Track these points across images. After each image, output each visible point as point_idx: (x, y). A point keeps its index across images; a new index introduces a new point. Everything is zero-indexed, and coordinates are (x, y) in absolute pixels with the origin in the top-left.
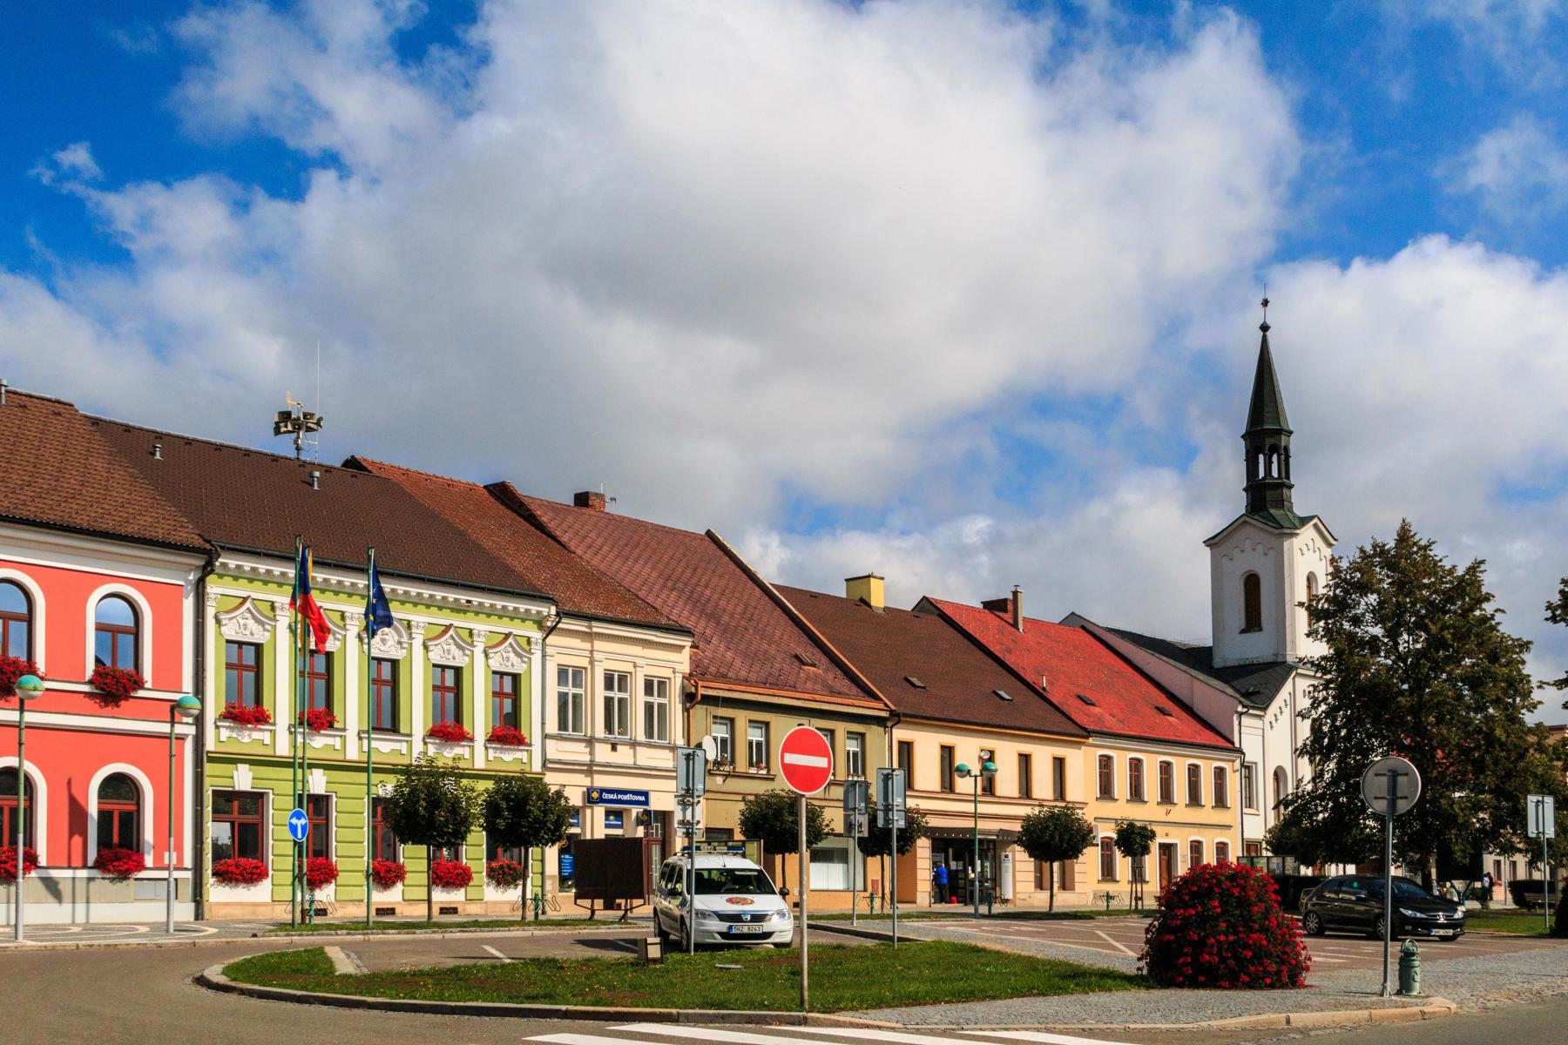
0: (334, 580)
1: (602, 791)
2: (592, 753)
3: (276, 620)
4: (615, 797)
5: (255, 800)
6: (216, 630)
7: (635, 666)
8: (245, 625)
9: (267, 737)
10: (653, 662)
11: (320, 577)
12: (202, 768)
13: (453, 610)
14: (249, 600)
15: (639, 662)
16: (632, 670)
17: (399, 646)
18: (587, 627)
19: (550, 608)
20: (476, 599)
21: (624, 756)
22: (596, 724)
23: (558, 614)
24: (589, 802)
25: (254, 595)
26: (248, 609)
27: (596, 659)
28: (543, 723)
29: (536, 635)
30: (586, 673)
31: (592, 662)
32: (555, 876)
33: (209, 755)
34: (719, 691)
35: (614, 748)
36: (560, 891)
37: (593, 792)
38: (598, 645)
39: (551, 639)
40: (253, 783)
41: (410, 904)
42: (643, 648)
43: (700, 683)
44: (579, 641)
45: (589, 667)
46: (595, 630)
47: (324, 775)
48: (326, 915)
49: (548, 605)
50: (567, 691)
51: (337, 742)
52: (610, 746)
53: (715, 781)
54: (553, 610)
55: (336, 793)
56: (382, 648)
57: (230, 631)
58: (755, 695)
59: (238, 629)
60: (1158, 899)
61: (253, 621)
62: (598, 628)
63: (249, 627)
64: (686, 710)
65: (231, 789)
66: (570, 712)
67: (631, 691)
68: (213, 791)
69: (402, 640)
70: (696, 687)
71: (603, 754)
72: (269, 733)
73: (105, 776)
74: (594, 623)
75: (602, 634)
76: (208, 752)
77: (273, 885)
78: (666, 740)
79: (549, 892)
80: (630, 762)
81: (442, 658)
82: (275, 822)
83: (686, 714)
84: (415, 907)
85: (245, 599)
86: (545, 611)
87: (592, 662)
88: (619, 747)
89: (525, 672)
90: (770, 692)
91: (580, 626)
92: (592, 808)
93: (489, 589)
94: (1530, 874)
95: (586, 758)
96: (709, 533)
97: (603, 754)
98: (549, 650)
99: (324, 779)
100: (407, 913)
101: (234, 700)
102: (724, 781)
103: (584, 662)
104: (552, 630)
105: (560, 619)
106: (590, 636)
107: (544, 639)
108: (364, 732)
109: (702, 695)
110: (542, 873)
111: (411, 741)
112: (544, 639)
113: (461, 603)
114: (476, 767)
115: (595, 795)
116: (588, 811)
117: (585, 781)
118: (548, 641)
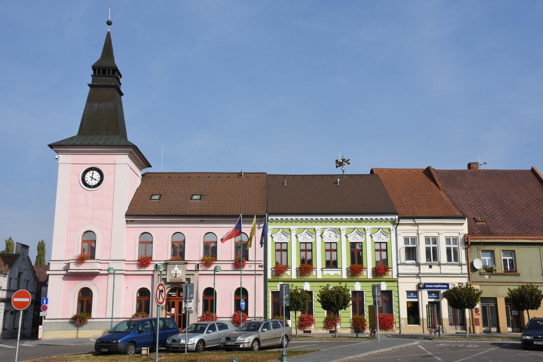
0: (344, 218)
1: (425, 284)
2: (420, 269)
3: (366, 234)
4: (432, 286)
5: (361, 293)
6: (321, 240)
7: (439, 234)
8: (380, 237)
9: (339, 273)
10: (426, 231)
11: (329, 218)
12: (266, 284)
13: (355, 222)
14: (306, 229)
15: (440, 232)
16: (438, 235)
17: (336, 237)
18: (413, 221)
19: (395, 217)
20: (364, 218)
21: (435, 269)
22: (422, 257)
23: (399, 218)
24: (419, 289)
25: (382, 227)
26: (381, 231)
27: (242, 231)
28: (397, 260)
29: (391, 227)
30: (417, 238)
31: (418, 234)
32: (405, 318)
33: (269, 280)
34: (481, 240)
35: (430, 267)
36: (408, 324)
37: (420, 285)
38: (421, 227)
39: (399, 227)
40: (361, 288)
41: (343, 329)
42: (412, 226)
43: (469, 238)
44: (411, 226)
45: (417, 236)
46: (417, 222)
47: (385, 284)
48: (311, 332)
49: (395, 216)
50: (450, 246)
51: (339, 273)
52: (428, 266)
53: (485, 277)
54: (397, 217)
55: (314, 290)
56: (330, 239)
57: (276, 240)
58: (502, 240)
59: (303, 238)
60: (327, 330)
61: (383, 235)
62: (418, 221)
63: (382, 237)
64: (466, 249)
65: (277, 291)
66: (411, 253)
67: (438, 244)
68: (271, 291)
69: (337, 235)
70: (468, 239)
71: (425, 269)
72: (289, 271)
73: (204, 289)
74: (416, 220)
75: (422, 223)
76: (268, 279)
77: (292, 322)
78: (437, 261)
79: (403, 324)
80: (438, 272)
81: (278, 240)
82: (366, 301)
83: (466, 250)
84: (345, 330)
85: (380, 228)
86: (393, 217)
87: (418, 234)
88: (433, 266)
89: (389, 241)
90: (512, 237)
91: (411, 221)
92: (421, 291)
93: (369, 213)
94: (519, 313)
95: (417, 272)
96: (533, 171)
97: (425, 269)
98: (398, 232)
99: (386, 285)
100: (342, 332)
101: (279, 261)
102: (489, 277)
103: (415, 235)
104: (398, 224)
105: (399, 220)
106: (417, 225)
107: (396, 228)
108: (348, 268)
109: (471, 242)
110: (399, 317)
111: (367, 270)
112: (396, 228)
113: (358, 220)
114: (368, 278)
115: (421, 286)
116: (420, 292)
117: (418, 281)
118: (397, 228)
